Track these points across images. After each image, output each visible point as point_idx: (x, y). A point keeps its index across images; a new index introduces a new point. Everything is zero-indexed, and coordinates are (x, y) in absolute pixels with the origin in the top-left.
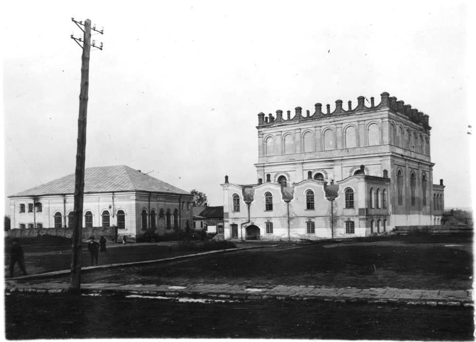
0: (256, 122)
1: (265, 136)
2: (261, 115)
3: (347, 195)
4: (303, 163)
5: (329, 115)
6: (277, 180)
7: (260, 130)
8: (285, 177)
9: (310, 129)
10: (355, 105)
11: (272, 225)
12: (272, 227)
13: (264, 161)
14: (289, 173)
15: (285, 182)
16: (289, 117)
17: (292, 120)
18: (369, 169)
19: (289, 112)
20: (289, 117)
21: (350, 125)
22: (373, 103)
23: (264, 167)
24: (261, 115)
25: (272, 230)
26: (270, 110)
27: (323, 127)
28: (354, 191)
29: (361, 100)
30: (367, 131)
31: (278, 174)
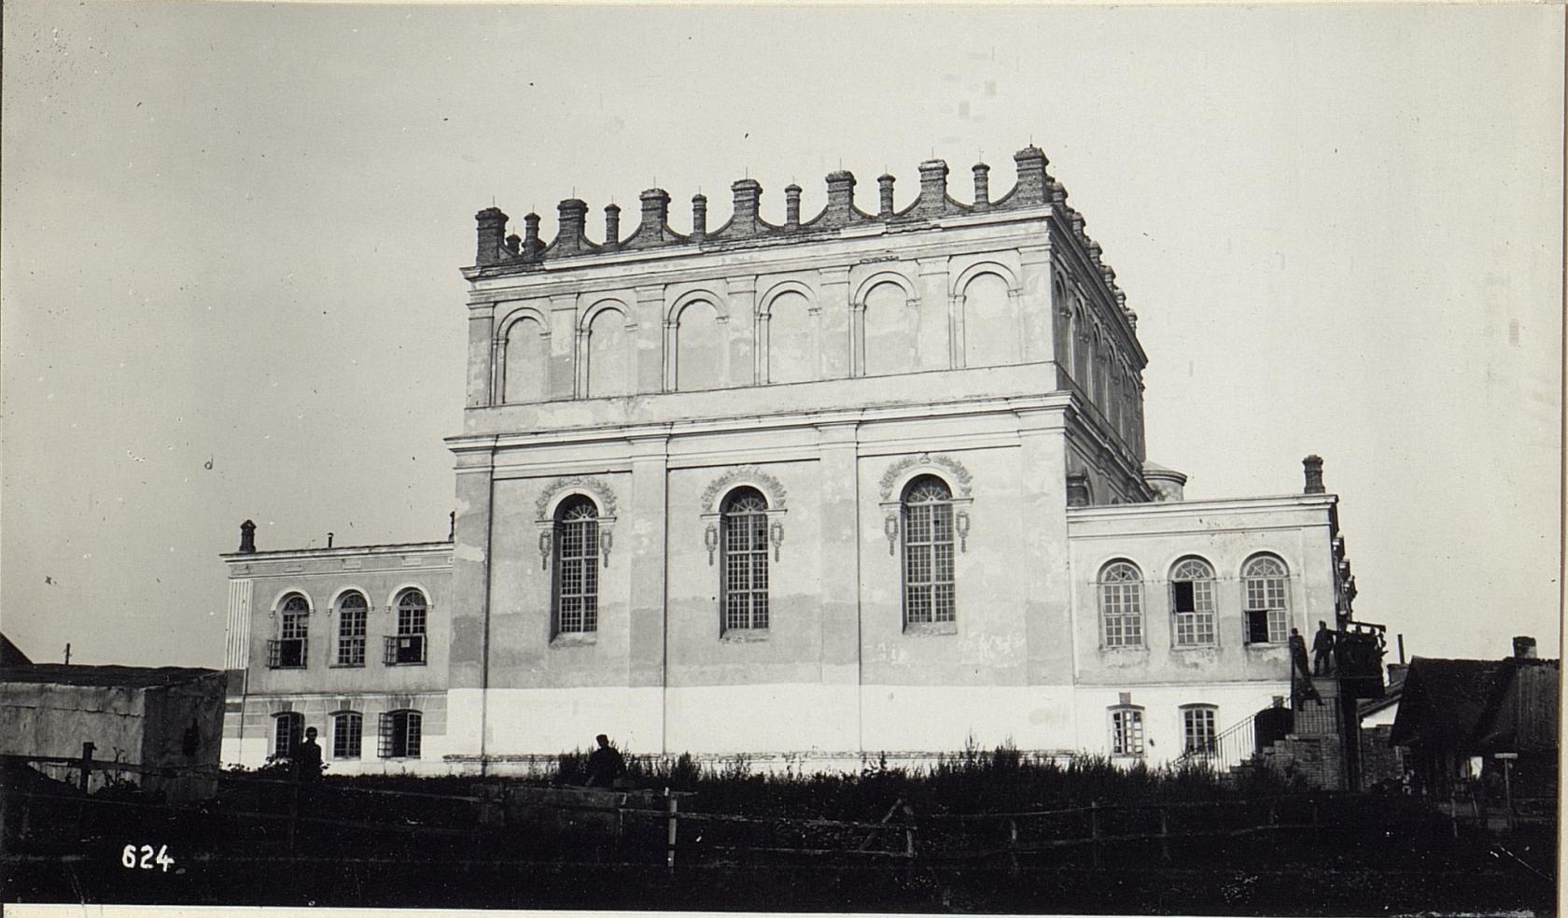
0: (467, 248)
1: (588, 299)
2: (492, 221)
3: (404, 615)
4: (861, 423)
5: (983, 204)
6: (550, 513)
7: (478, 285)
8: (763, 499)
9: (534, 304)
10: (630, 222)
11: (419, 724)
12: (419, 731)
13: (488, 422)
14: (964, 459)
15: (592, 526)
16: (794, 211)
17: (999, 205)
18: (971, 470)
19: (613, 211)
20: (794, 211)
21: (520, 314)
22: (703, 217)
23: (495, 450)
24: (492, 221)
25: (359, 746)
26: (530, 200)
27: (500, 306)
28: (429, 602)
29: (657, 203)
30: (673, 331)
31: (906, 464)
